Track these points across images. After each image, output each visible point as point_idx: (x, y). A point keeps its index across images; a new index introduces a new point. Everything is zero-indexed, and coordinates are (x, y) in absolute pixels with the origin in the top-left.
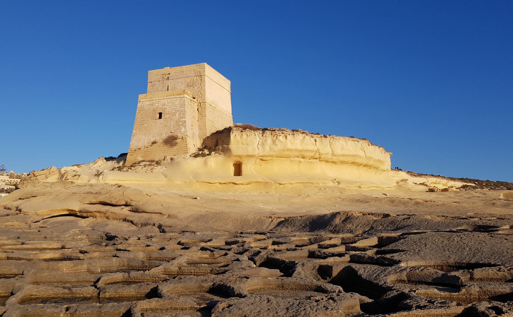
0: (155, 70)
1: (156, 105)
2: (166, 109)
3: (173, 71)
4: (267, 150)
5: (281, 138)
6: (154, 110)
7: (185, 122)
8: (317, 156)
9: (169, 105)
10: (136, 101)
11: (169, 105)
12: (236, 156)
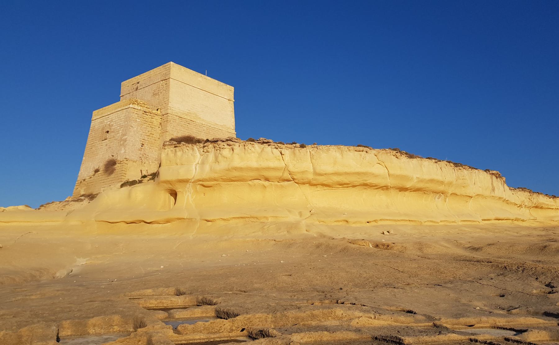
1: (106, 121)
2: (112, 125)
4: (207, 172)
6: (103, 129)
7: (125, 140)
8: (287, 175)
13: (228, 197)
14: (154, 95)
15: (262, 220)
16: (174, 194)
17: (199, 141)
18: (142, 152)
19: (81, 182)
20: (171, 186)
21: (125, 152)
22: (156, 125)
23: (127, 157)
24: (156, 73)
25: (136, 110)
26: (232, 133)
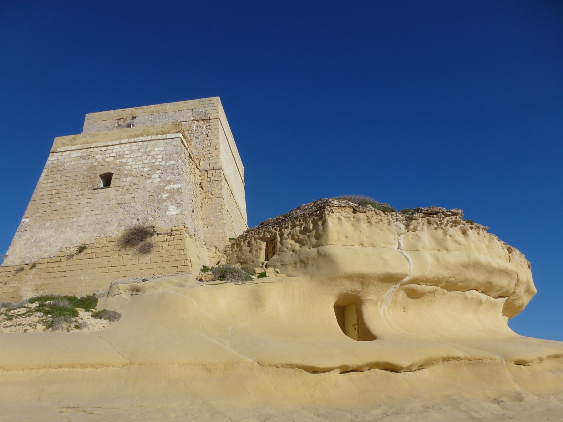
2: (125, 164)
9: (134, 155)
10: (45, 150)
11: (134, 155)
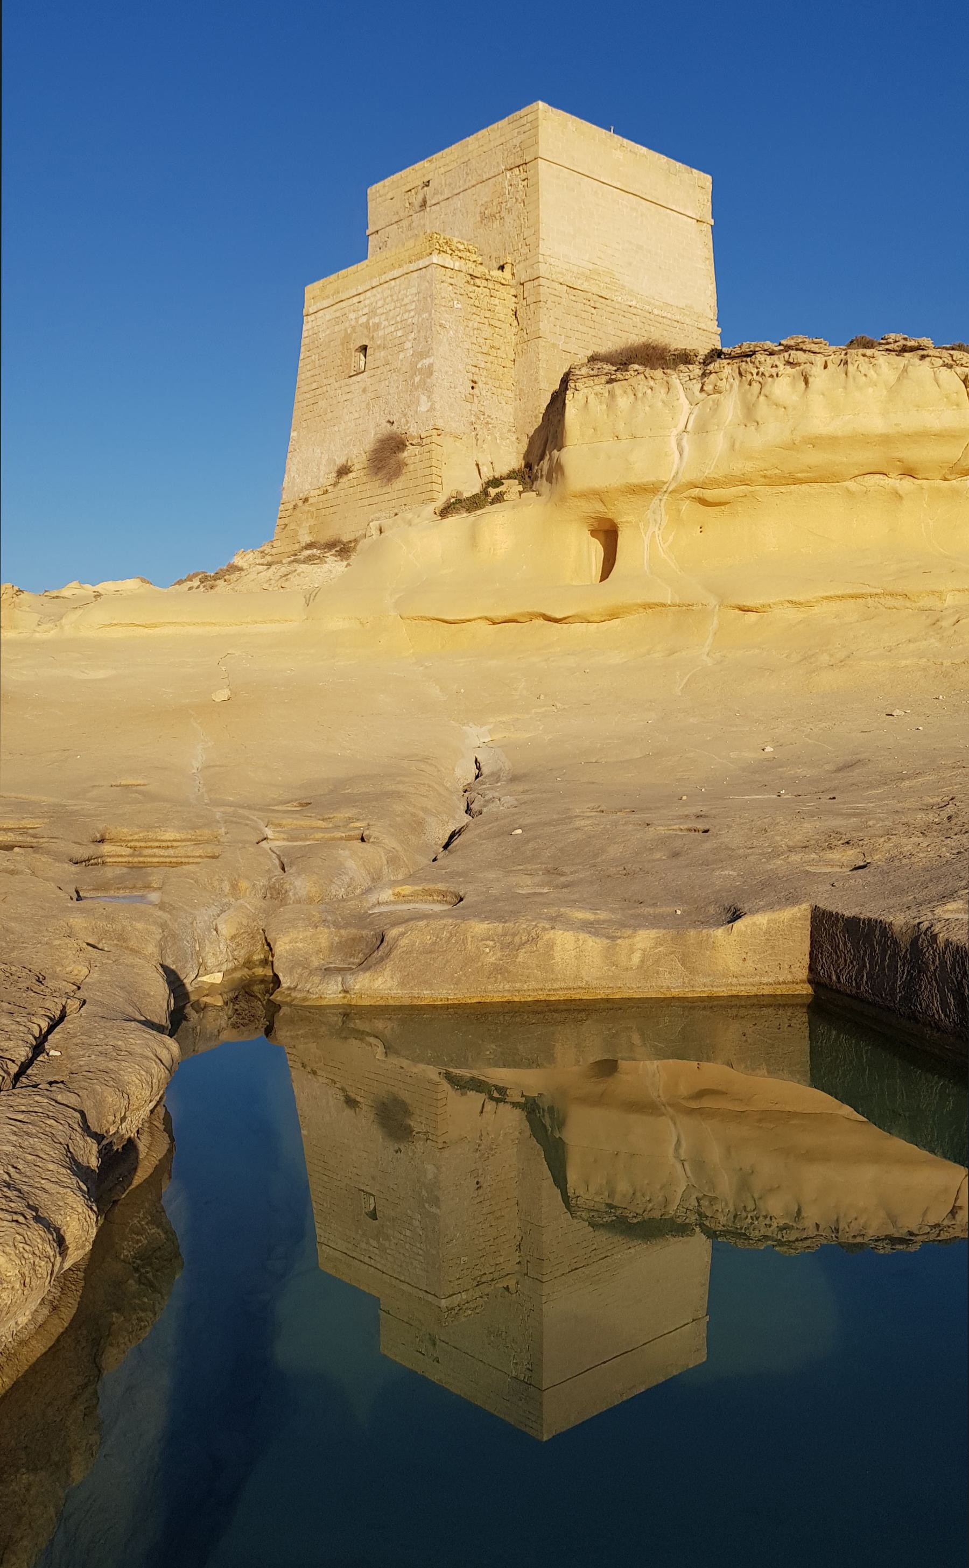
0: (387, 181)
1: (352, 316)
2: (377, 326)
3: (438, 167)
4: (718, 455)
5: (784, 386)
6: (347, 339)
7: (429, 371)
12: (584, 495)
13: (778, 532)
14: (486, 218)
15: (925, 602)
16: (608, 535)
17: (685, 358)
18: (475, 408)
19: (295, 507)
20: (599, 507)
21: (432, 409)
22: (502, 317)
23: (440, 423)
24: (488, 144)
25: (449, 273)
26: (702, 333)
